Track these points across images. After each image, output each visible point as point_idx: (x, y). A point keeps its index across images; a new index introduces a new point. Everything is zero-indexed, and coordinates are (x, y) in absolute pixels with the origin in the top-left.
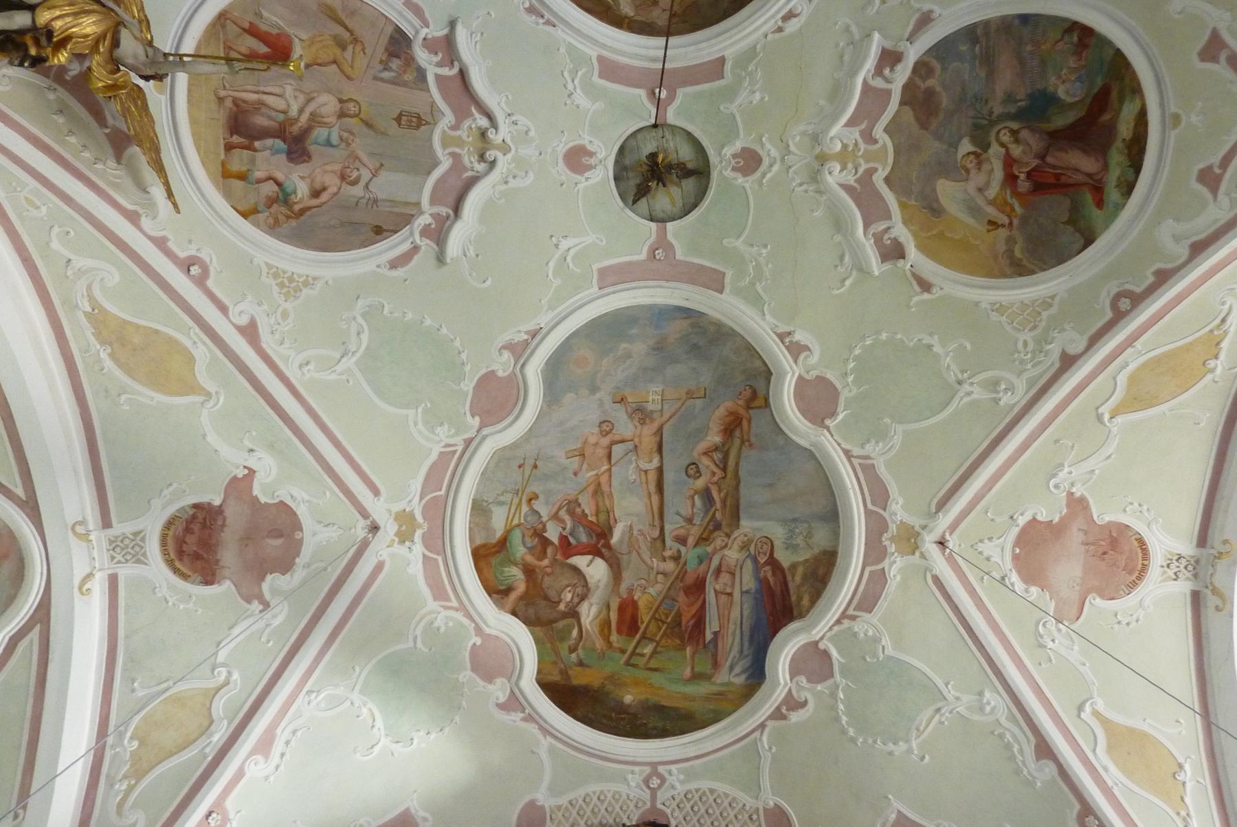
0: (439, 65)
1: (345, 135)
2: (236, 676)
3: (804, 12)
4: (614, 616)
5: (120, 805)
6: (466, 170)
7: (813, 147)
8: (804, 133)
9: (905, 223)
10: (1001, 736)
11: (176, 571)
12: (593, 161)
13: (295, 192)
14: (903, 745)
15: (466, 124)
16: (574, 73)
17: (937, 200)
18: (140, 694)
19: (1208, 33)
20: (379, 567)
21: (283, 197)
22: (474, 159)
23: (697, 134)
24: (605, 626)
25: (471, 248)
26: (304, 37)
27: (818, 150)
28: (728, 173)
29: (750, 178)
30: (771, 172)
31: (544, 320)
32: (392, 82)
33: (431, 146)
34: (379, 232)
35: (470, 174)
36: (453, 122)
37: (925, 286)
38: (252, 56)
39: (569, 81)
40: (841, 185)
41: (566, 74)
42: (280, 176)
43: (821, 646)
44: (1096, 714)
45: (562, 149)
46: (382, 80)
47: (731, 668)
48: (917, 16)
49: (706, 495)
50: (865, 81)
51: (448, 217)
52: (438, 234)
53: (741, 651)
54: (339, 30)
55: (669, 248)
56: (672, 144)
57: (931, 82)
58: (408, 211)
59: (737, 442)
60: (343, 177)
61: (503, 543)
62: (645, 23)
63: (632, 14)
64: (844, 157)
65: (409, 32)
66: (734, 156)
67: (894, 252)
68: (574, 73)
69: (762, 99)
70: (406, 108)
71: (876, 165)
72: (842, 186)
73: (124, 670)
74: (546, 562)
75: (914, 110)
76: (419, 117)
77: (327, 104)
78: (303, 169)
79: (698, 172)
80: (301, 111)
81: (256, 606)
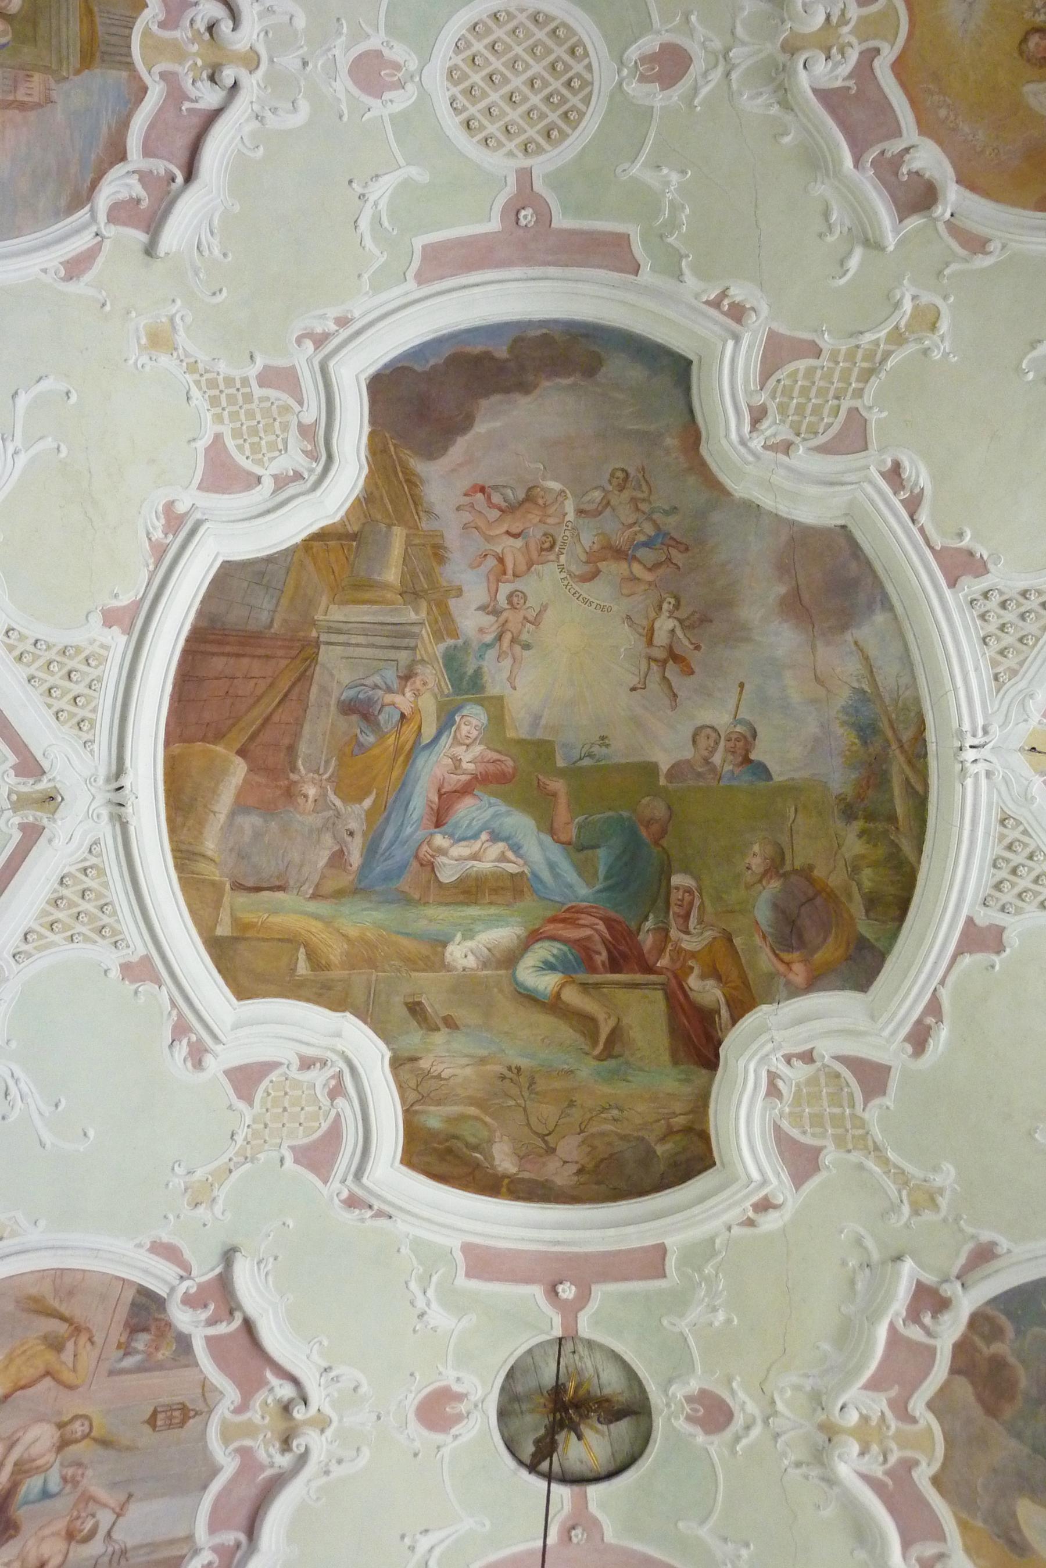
0: (212, 1322)
1: (70, 1472)
3: (790, 1203)
6: (262, 1468)
7: (814, 1410)
8: (797, 1388)
9: (967, 1550)
12: (463, 1407)
16: (425, 1281)
17: (1019, 1530)
22: (274, 1450)
23: (629, 1357)
25: (215, 241)
27: (821, 1417)
28: (680, 1424)
29: (716, 1439)
30: (703, 79)
32: (140, 1369)
33: (205, 1447)
35: (268, 1473)
39: (419, 1294)
40: (815, 91)
41: (413, 1285)
45: (412, 1401)
48: (968, 1248)
50: (892, 1328)
51: (238, 1545)
55: (593, 1526)
56: (589, 1364)
57: (998, 1348)
58: (174, 1552)
60: (70, 1536)
62: (536, 1182)
63: (513, 1170)
64: (866, 1433)
65: (162, 1291)
66: (643, 59)
67: (918, 198)
68: (425, 1281)
69: (729, 1321)
72: (867, 1478)
75: (973, 1383)
76: (184, 1408)
79: (632, 1410)
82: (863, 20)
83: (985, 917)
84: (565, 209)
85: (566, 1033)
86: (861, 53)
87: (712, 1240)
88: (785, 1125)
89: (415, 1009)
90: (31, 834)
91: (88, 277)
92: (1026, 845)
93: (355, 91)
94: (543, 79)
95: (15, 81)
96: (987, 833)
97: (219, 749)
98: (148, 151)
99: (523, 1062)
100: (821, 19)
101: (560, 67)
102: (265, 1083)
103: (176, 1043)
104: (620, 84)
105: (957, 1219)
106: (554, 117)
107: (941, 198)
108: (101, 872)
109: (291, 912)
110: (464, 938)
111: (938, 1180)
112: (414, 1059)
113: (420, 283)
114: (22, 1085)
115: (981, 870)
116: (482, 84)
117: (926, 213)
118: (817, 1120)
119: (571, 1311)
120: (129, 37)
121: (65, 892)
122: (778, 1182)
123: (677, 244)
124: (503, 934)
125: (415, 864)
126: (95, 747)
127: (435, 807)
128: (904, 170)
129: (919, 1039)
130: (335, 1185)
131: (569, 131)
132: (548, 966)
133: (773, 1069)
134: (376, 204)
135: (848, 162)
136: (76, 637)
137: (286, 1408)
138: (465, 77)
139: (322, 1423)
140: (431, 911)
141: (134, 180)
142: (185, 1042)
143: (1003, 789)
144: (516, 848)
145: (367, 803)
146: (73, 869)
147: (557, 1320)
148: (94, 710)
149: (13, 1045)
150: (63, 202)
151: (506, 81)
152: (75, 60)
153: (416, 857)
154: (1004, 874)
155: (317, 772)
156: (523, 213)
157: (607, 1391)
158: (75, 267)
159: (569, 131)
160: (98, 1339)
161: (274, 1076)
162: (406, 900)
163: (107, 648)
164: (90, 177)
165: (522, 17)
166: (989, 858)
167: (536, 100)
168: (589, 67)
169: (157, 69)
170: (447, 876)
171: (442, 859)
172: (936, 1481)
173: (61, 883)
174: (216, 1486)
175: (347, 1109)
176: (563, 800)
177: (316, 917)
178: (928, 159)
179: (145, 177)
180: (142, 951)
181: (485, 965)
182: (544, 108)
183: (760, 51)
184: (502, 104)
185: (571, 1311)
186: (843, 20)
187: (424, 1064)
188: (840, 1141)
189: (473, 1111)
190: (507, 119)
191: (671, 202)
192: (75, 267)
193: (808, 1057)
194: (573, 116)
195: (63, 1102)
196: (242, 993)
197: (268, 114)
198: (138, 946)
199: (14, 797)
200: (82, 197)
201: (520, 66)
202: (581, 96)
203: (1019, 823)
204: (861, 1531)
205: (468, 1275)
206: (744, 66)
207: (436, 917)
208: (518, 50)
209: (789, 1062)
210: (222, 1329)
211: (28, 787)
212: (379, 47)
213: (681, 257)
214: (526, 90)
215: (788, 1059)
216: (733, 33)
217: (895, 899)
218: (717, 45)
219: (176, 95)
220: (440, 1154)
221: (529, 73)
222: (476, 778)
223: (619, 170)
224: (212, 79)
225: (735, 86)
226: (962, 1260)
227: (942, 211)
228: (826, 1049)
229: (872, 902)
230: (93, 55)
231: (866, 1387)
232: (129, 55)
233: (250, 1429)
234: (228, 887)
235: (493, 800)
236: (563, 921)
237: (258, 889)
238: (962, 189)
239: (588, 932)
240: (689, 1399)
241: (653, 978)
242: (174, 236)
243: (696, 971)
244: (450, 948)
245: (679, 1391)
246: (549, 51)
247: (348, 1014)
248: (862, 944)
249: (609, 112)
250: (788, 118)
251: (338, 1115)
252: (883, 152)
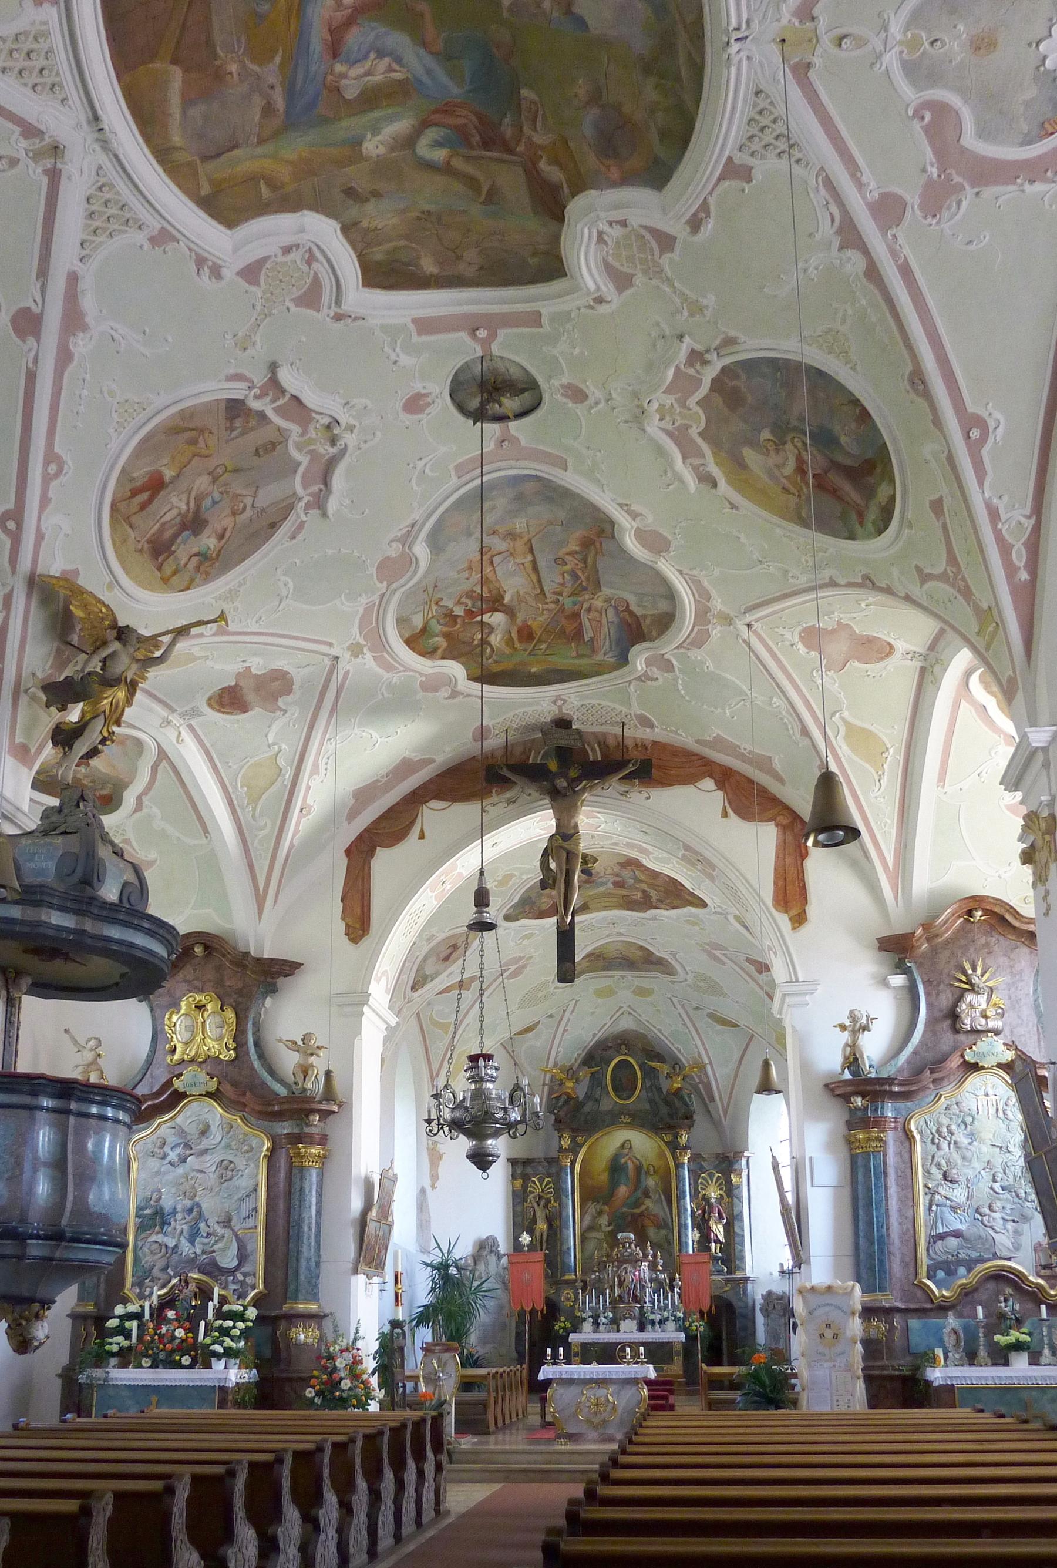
0: (273, 401)
2: (284, 746)
3: (615, 301)
4: (514, 635)
5: (253, 816)
6: (324, 456)
9: (717, 464)
10: (782, 719)
11: (223, 713)
12: (429, 400)
13: (209, 548)
14: (719, 710)
15: (311, 428)
18: (235, 767)
19: (937, 496)
20: (346, 674)
21: (204, 557)
24: (510, 642)
26: (165, 462)
28: (559, 397)
31: (417, 515)
32: (242, 434)
34: (274, 526)
36: (300, 431)
37: (733, 506)
38: (143, 507)
41: (386, 349)
42: (195, 550)
43: (666, 656)
44: (843, 719)
45: (400, 404)
46: (233, 439)
47: (605, 654)
48: (722, 336)
49: (574, 575)
51: (321, 490)
52: (319, 503)
53: (611, 648)
54: (188, 435)
59: (593, 552)
60: (234, 514)
61: (425, 630)
69: (582, 353)
71: (690, 423)
73: (220, 760)
74: (458, 626)
77: (202, 483)
78: (207, 531)
80: (188, 504)
81: (279, 713)
83: (740, 158)
85: (458, 187)
87: (569, 313)
88: (610, 259)
89: (350, 192)
90: (54, 177)
92: (771, 113)
96: (745, 101)
97: (158, 65)
99: (431, 207)
102: (264, 271)
103: (201, 272)
105: (716, 323)
108: (112, 186)
109: (246, 161)
110: (374, 135)
111: (705, 302)
112: (356, 224)
114: (120, 331)
115: (739, 127)
118: (630, 259)
119: (486, 343)
121: (93, 208)
122: (608, 289)
124: (401, 126)
125: (325, 92)
126: (70, 102)
127: (330, 43)
129: (695, 224)
130: (325, 310)
132: (437, 144)
133: (601, 229)
136: (21, 24)
137: (328, 427)
139: (351, 428)
140: (344, 123)
142: (206, 268)
143: (759, 71)
144: (399, 60)
145: (278, 60)
146: (92, 191)
147: (479, 348)
148: (58, 74)
149: (104, 311)
153: (324, 85)
154: (754, 130)
155: (233, 52)
157: (514, 377)
160: (214, 430)
161: (268, 265)
162: (325, 121)
163: (46, 23)
166: (745, 120)
170: (351, 94)
171: (344, 82)
172: (700, 434)
173: (88, 202)
174: (301, 470)
175: (321, 268)
176: (428, 17)
177: (265, 156)
180: (159, 226)
181: (392, 149)
185: (486, 343)
187: (364, 224)
188: (645, 272)
189: (403, 243)
193: (623, 223)
195: (147, 330)
196: (230, 223)
198: (155, 224)
199: (31, 154)
203: (768, 96)
204: (660, 451)
205: (419, 334)
207: (348, 126)
209: (611, 225)
211: (36, 144)
215: (611, 224)
217: (680, 132)
220: (385, 273)
222: (356, 9)
226: (718, 342)
228: (634, 222)
229: (663, 134)
231: (664, 392)
233: (311, 442)
234: (198, 161)
235: (373, 24)
236: (445, 112)
237: (218, 155)
239: (464, 121)
240: (563, 386)
241: (514, 158)
243: (544, 159)
244: (365, 145)
245: (555, 382)
247: (305, 212)
248: (656, 161)
251: (316, 274)
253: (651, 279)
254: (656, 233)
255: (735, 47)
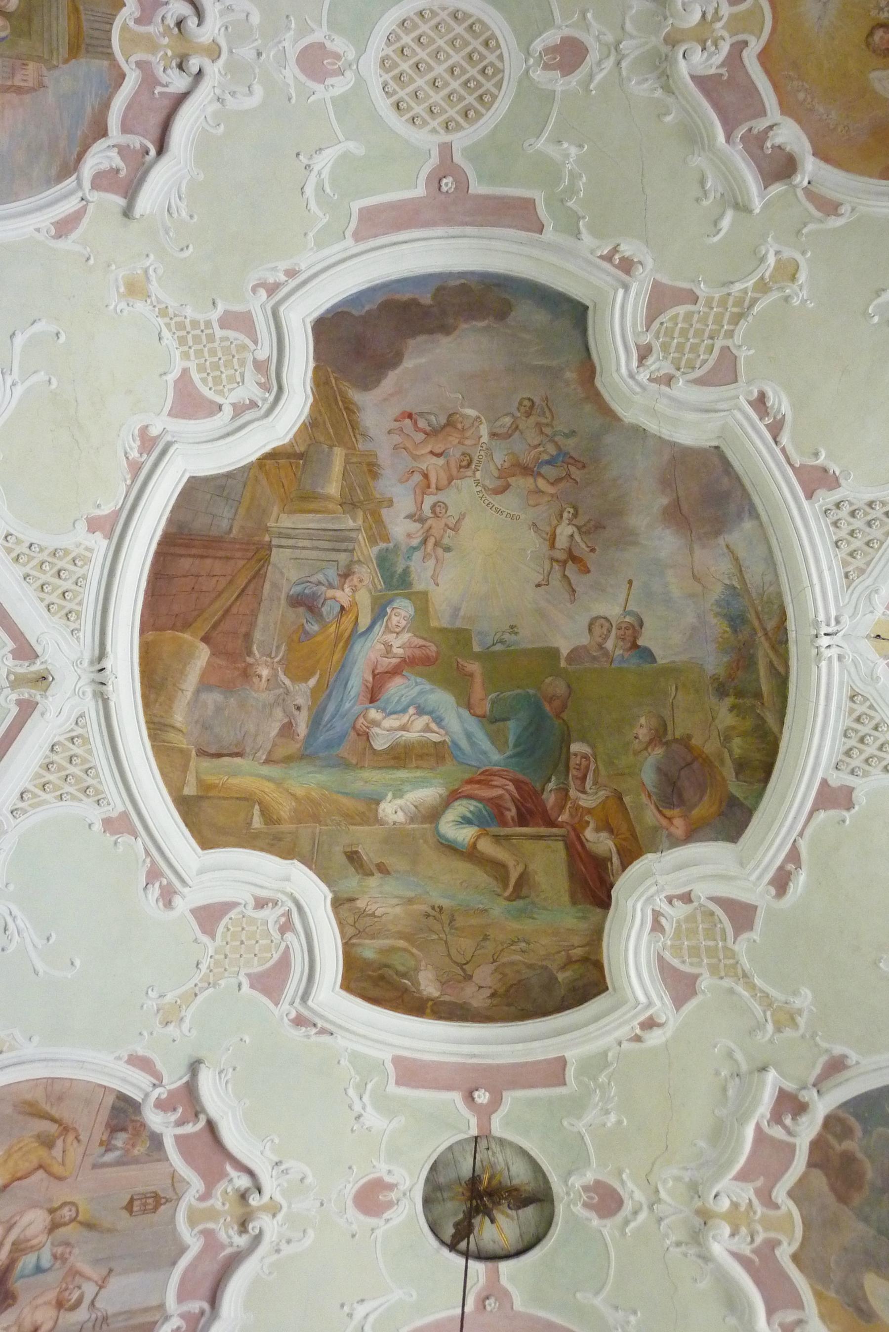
0: (180, 1123)
1: (59, 1250)
3: (671, 1022)
6: (223, 1247)
7: (692, 1198)
8: (677, 1179)
9: (822, 1317)
12: (393, 1196)
16: (361, 1089)
17: (866, 1300)
22: (233, 1232)
23: (535, 1153)
25: (183, 205)
27: (698, 1204)
28: (578, 1209)
29: (609, 1222)
30: (598, 67)
32: (119, 1163)
33: (175, 1229)
35: (228, 1251)
39: (356, 1099)
40: (693, 77)
41: (351, 1092)
45: (350, 1191)
48: (822, 1060)
51: (202, 1313)
55: (504, 1296)
56: (501, 1159)
57: (848, 1145)
58: (148, 1318)
60: (60, 1305)
62: (455, 1004)
63: (436, 994)
64: (736, 1218)
65: (137, 1096)
66: (547, 50)
67: (780, 168)
68: (361, 1089)
69: (619, 1122)
70: (140, 1189)
72: (737, 1256)
75: (827, 1175)
76: (156, 1196)
79: (537, 1198)
82: (733, 17)
83: (837, 779)
84: (480, 178)
85: (481, 877)
86: (732, 45)
87: (605, 1054)
88: (667, 955)
89: (353, 857)
90: (27, 708)
91: (75, 235)
92: (872, 718)
93: (302, 78)
94: (461, 67)
95: (13, 69)
96: (839, 708)
97: (186, 636)
98: (125, 129)
99: (445, 902)
100: (697, 16)
101: (476, 57)
102: (225, 920)
103: (150, 886)
104: (527, 71)
105: (814, 1035)
106: (470, 99)
107: (799, 169)
108: (86, 741)
109: (247, 775)
110: (395, 797)
111: (797, 1003)
112: (352, 900)
113: (357, 241)
114: (19, 922)
115: (834, 739)
116: (409, 71)
117: (787, 181)
118: (694, 951)
119: (485, 1113)
120: (110, 31)
121: (55, 758)
122: (661, 1004)
123: (575, 207)
124: (427, 794)
125: (353, 734)
126: (81, 634)
127: (370, 685)
128: (769, 144)
129: (781, 882)
130: (285, 1006)
131: (483, 111)
132: (466, 821)
133: (657, 908)
134: (319, 173)
135: (721, 137)
136: (65, 541)
137: (243, 1196)
138: (395, 65)
139: (273, 1209)
140: (366, 774)
141: (114, 153)
142: (157, 885)
143: (853, 670)
144: (439, 721)
145: (312, 682)
146: (62, 739)
147: (474, 1121)
148: (80, 603)
149: (11, 887)
150: (54, 172)
151: (430, 68)
152: (64, 51)
153: (354, 728)
155: (269, 655)
156: (444, 181)
157: (516, 1182)
158: (64, 227)
159: (483, 111)
160: (84, 1137)
161: (233, 914)
162: (345, 765)
163: (91, 550)
164: (76, 150)
165: (444, 15)
166: (840, 729)
167: (455, 85)
168: (501, 57)
169: (133, 59)
170: (380, 744)
171: (375, 730)
172: (795, 1258)
173: (52, 750)
174: (184, 1262)
175: (295, 942)
176: (478, 680)
177: (269, 779)
178: (789, 135)
179: (123, 151)
180: (120, 808)
181: (412, 820)
182: (463, 92)
183: (646, 43)
184: (426, 88)
185: (485, 1113)
186: (717, 17)
187: (361, 904)
188: (714, 970)
189: (402, 943)
190: (431, 101)
191: (570, 172)
192: (64, 227)
193: (687, 898)
194: (487, 98)
195: (54, 936)
196: (206, 843)
197: (228, 97)
198: (117, 804)
200: (69, 167)
201: (442, 56)
202: (493, 81)
203: (866, 699)
205: (398, 1083)
206: (632, 56)
207: (370, 779)
208: (441, 42)
209: (670, 902)
210: (189, 1129)
211: (23, 668)
212: (322, 40)
213: (579, 218)
214: (447, 77)
215: (670, 900)
216: (623, 28)
217: (761, 763)
218: (610, 38)
219: (149, 80)
220: (374, 981)
221: (450, 62)
222: (405, 661)
223: (526, 145)
224: (180, 67)
225: (624, 73)
226: (817, 1070)
227: (801, 179)
228: (702, 891)
229: (741, 766)
230: (79, 47)
231: (736, 1178)
232: (110, 47)
233: (212, 1214)
234: (194, 753)
235: (419, 680)
236: (479, 782)
237: (219, 755)
238: (818, 161)
239: (500, 792)
240: (586, 1189)
241: (555, 830)
242: (148, 200)
243: (592, 825)
244: (383, 805)
245: (577, 1182)
246: (467, 44)
247: (295, 861)
248: (733, 802)
249: (517, 95)
250: (670, 100)
252: (750, 130)
253: (722, 978)
254: (731, 906)
255: (824, 641)
